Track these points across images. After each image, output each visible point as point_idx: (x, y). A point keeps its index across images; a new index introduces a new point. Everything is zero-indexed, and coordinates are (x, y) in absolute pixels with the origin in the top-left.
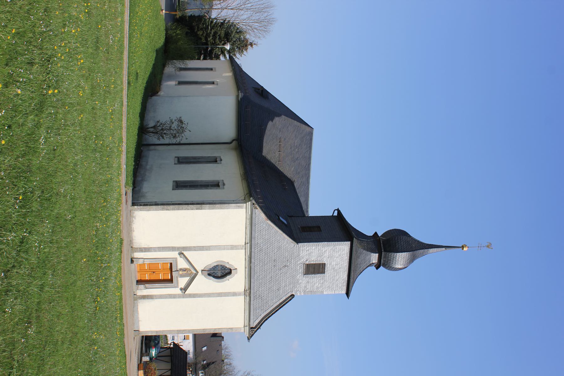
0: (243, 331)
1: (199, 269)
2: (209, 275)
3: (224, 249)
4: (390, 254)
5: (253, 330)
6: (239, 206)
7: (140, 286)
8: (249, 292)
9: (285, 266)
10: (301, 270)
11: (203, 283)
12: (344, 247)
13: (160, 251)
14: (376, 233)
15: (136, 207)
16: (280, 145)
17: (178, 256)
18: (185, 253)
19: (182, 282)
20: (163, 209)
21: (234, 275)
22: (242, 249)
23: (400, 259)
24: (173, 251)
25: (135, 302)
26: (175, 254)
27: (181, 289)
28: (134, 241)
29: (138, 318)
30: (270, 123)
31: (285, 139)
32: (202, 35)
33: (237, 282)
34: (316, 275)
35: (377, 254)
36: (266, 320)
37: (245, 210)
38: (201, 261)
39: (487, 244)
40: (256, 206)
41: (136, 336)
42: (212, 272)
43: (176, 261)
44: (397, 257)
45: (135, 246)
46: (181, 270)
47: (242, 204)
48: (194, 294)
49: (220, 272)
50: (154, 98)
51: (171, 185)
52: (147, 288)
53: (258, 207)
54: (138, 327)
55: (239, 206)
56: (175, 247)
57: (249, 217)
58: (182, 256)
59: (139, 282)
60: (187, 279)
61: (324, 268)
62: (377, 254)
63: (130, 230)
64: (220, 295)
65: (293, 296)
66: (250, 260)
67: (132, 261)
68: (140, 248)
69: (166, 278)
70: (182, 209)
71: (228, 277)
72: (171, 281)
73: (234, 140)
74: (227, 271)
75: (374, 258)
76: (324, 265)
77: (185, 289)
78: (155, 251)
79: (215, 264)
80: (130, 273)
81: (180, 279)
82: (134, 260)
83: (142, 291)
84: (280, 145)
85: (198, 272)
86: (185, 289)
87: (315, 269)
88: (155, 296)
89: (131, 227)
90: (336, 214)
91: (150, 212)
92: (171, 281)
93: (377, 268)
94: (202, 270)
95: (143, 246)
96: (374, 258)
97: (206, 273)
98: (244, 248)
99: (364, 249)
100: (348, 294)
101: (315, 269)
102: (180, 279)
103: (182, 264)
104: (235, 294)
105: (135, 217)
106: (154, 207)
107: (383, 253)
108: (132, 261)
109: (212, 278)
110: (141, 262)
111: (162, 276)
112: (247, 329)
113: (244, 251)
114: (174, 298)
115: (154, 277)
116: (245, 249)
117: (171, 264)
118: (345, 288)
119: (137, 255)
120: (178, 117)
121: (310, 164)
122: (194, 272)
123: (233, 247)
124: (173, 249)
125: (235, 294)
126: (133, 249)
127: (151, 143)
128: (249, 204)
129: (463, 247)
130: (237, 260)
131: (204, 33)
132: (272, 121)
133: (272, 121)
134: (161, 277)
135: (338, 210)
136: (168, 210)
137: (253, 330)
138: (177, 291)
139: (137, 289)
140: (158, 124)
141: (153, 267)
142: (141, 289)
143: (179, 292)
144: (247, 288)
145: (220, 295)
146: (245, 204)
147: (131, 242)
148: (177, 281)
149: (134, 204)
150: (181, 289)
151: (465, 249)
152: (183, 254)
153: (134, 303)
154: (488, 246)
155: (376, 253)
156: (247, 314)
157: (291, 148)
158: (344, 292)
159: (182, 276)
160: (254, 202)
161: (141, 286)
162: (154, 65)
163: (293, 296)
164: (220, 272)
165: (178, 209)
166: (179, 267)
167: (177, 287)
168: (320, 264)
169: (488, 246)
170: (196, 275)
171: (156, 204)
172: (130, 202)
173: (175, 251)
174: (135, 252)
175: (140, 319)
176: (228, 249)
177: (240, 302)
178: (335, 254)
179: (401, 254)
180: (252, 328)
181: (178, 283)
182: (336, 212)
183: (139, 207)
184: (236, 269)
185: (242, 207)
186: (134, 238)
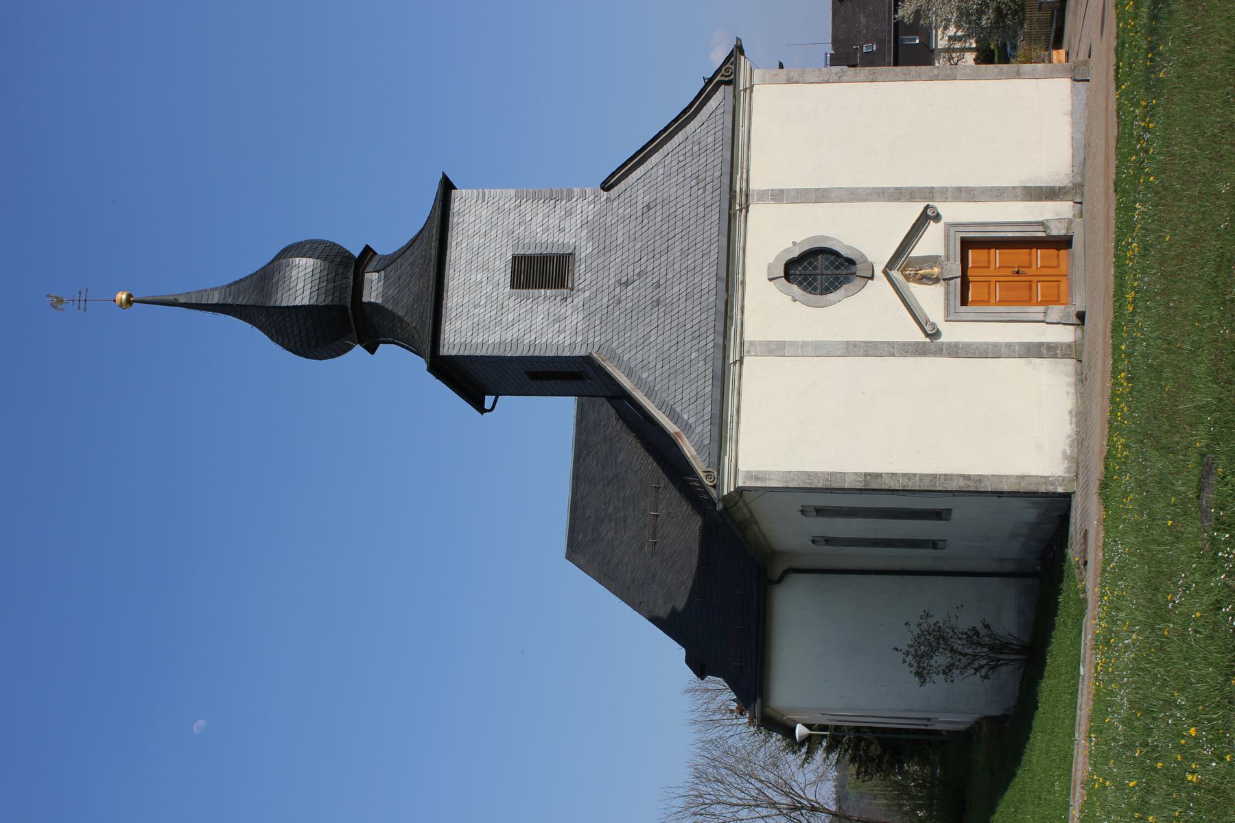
0: (757, 73)
1: (881, 281)
2: (851, 262)
3: (804, 344)
4: (327, 302)
5: (725, 77)
6: (757, 478)
7: (1063, 233)
8: (734, 204)
9: (627, 284)
10: (581, 273)
11: (871, 234)
12: (463, 333)
13: (996, 345)
14: (372, 350)
15: (1060, 490)
16: (654, 535)
17: (942, 326)
18: (921, 337)
19: (931, 243)
20: (980, 479)
21: (777, 259)
22: (752, 343)
23: (302, 284)
24: (956, 345)
25: (1078, 179)
26: (952, 333)
27: (937, 218)
28: (1072, 380)
29: (1074, 124)
30: (680, 605)
31: (641, 548)
32: (869, 744)
33: (770, 236)
34: (538, 251)
35: (365, 299)
36: (684, 112)
37: (741, 467)
38: (869, 309)
39: (64, 306)
40: (707, 482)
41: (1085, 63)
42: (843, 271)
43: (947, 313)
44: (307, 293)
45: (1068, 365)
46: (936, 280)
47: (748, 484)
48: (899, 200)
49: (819, 270)
50: (994, 711)
51: (954, 515)
52: (1042, 224)
53: (702, 475)
54: (1074, 93)
55: (757, 478)
56: (950, 355)
57: (729, 446)
58: (928, 328)
59: (1064, 243)
60: (921, 249)
61: (513, 272)
62: (365, 299)
63: (1081, 416)
64: (821, 196)
65: (607, 186)
66: (727, 311)
67: (1081, 316)
68: (1055, 356)
69: (982, 253)
70: (923, 477)
71: (795, 254)
72: (967, 244)
73: (779, 581)
74: (799, 270)
75: (374, 289)
76: (516, 283)
77: (926, 218)
78: (1009, 345)
79: (831, 296)
80: (1091, 274)
81: (940, 251)
82: (1074, 320)
83: (1054, 215)
84: (654, 535)
85: (885, 272)
86: (926, 218)
87: (539, 271)
88: (1016, 198)
89: (1078, 424)
90: (489, 400)
91: (1019, 473)
92: (967, 244)
93: (368, 250)
94: (872, 278)
95: (1044, 364)
96: (374, 289)
97: (860, 269)
98: (746, 347)
99: (401, 319)
100: (447, 187)
101: (539, 271)
102: (940, 251)
103: (931, 298)
104: (778, 196)
105: (1065, 457)
106: (1006, 487)
107: (349, 300)
108: (1081, 316)
109: (844, 253)
110: (1055, 312)
111: (993, 266)
112: (743, 83)
113: (747, 338)
114: (959, 190)
115: (1021, 255)
116: (742, 344)
117: (964, 302)
118: (456, 206)
119: (1065, 335)
120: (928, 685)
121: (577, 460)
122: (895, 274)
123: (777, 349)
124: (956, 351)
125: (778, 196)
126: (1073, 352)
127: (1011, 580)
128: (727, 489)
129: (129, 302)
130: (767, 307)
131: (866, 752)
132: (674, 610)
133: (674, 610)
134: (997, 255)
135: (482, 410)
136: (964, 476)
137: (725, 77)
138: (951, 212)
139: (1070, 221)
140: (983, 672)
141: (1021, 294)
142: (1060, 220)
143: (943, 208)
144: (740, 218)
145: (821, 196)
146: (740, 484)
147: (1082, 379)
148: (947, 246)
149: (1068, 496)
150: (937, 218)
151: (122, 296)
152: (927, 335)
153: (1083, 176)
154: (61, 301)
155: (370, 304)
156: (742, 131)
157: (625, 518)
158: (459, 200)
159: (932, 260)
160: (713, 492)
161: (1057, 231)
162: (993, 813)
163: (607, 186)
164: (819, 270)
165: (935, 476)
166: (938, 290)
167: (949, 226)
168: (527, 287)
169: (61, 301)
170: (891, 265)
171: (1000, 494)
172: (1077, 503)
173: (949, 344)
174: (1069, 346)
175: (1068, 119)
176: (792, 344)
177: (764, 169)
178: (483, 313)
179: (298, 302)
180: (728, 83)
181: (947, 237)
182: (488, 405)
183: (1051, 489)
184: (771, 280)
185: (751, 475)
186: (1072, 390)
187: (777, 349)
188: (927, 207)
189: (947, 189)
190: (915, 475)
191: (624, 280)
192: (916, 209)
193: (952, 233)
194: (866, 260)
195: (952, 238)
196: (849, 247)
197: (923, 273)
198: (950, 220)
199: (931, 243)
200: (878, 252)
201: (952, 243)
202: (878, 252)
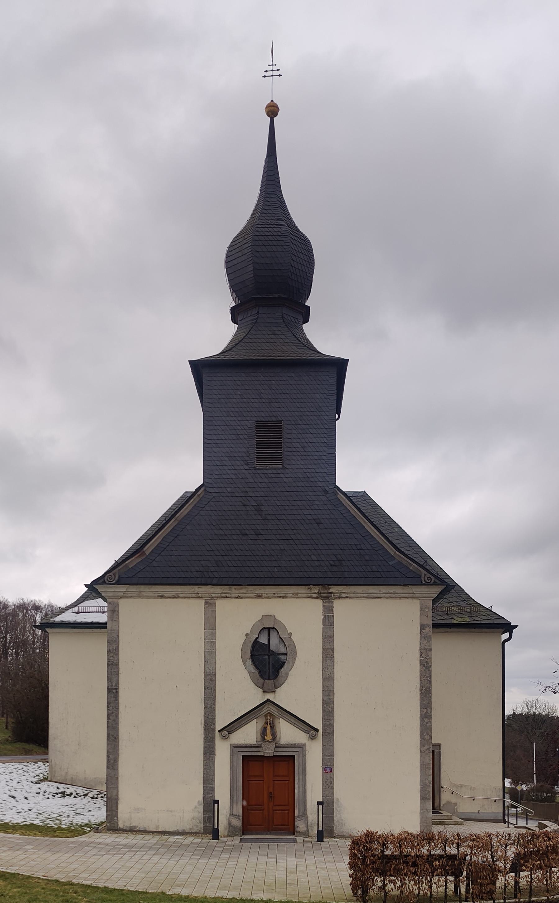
11: (299, 691)
13: (213, 780)
33: (298, 615)
38: (239, 691)
49: (267, 660)
64: (328, 654)
79: (249, 662)
94: (264, 692)
95: (199, 813)
103: (249, 734)
123: (210, 625)
124: (209, 752)
130: (240, 615)
145: (328, 654)
164: (267, 660)
173: (214, 747)
187: (210, 625)
188: (317, 730)
189: (109, 660)
190: (117, 724)
191: (262, 508)
192: (318, 723)
193: (297, 749)
194: (276, 687)
195: (294, 749)
196: (287, 675)
197: (269, 729)
198: (308, 748)
199: (288, 733)
200: (284, 696)
201: (290, 749)
202: (284, 696)
